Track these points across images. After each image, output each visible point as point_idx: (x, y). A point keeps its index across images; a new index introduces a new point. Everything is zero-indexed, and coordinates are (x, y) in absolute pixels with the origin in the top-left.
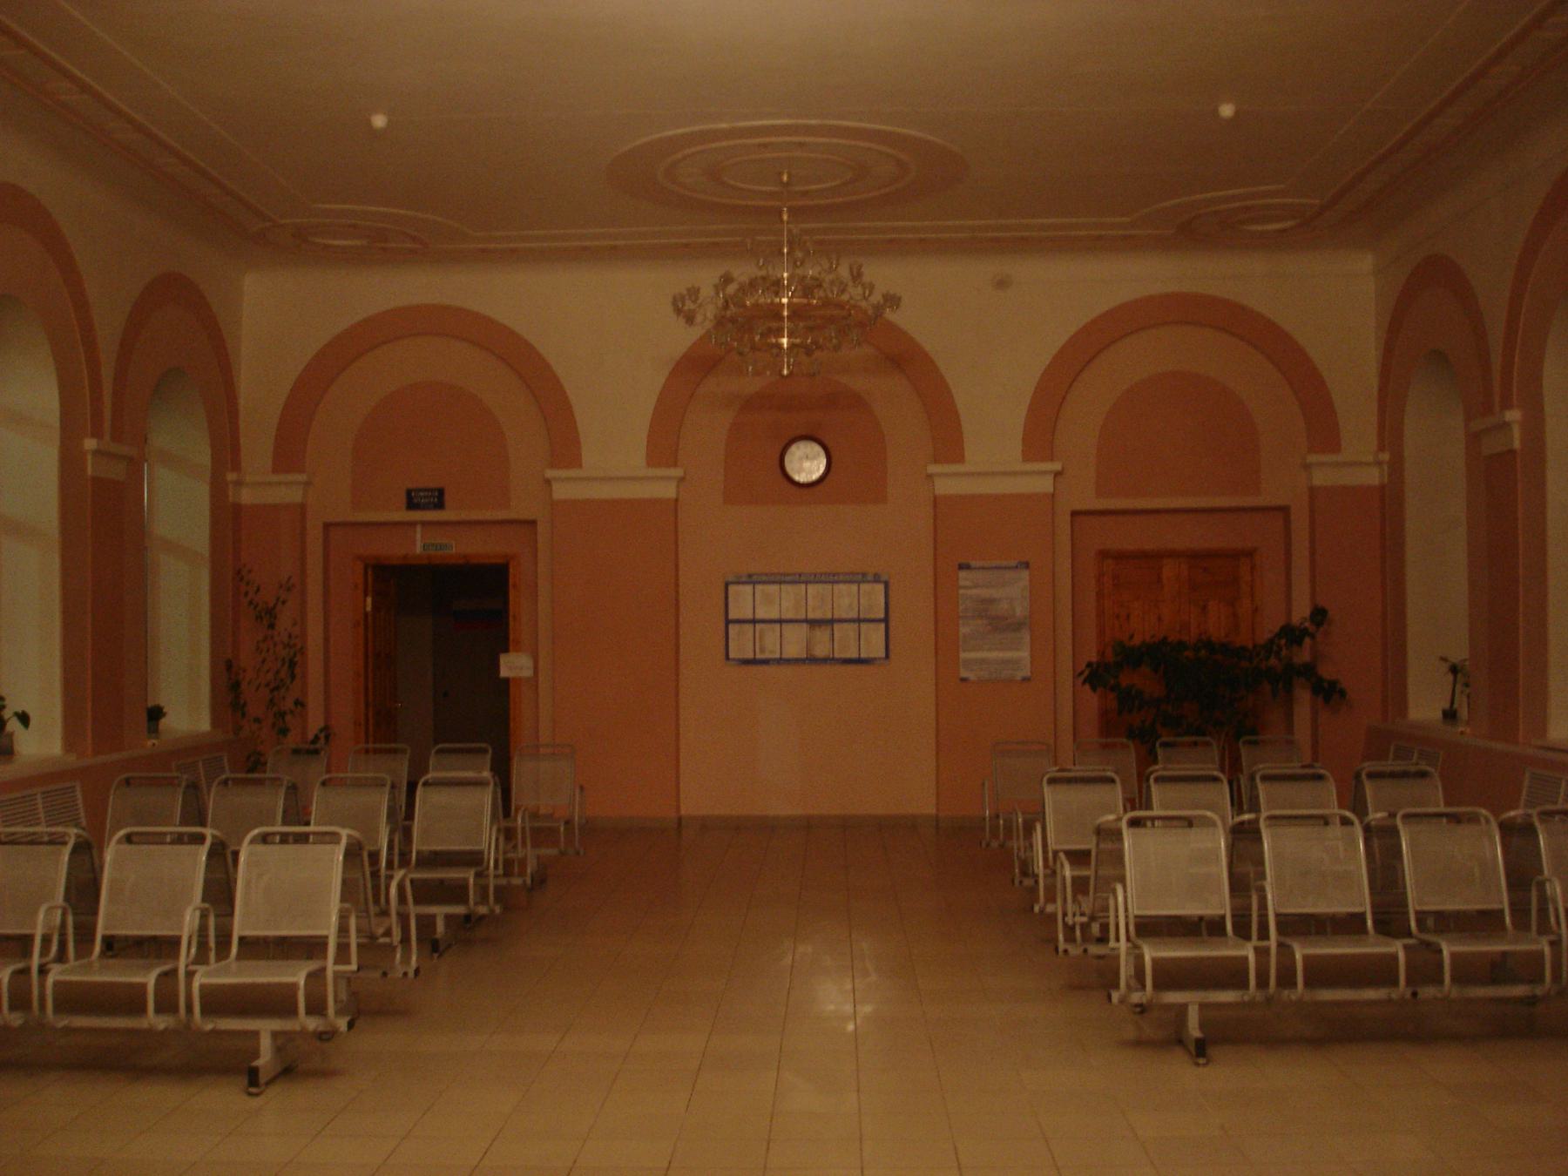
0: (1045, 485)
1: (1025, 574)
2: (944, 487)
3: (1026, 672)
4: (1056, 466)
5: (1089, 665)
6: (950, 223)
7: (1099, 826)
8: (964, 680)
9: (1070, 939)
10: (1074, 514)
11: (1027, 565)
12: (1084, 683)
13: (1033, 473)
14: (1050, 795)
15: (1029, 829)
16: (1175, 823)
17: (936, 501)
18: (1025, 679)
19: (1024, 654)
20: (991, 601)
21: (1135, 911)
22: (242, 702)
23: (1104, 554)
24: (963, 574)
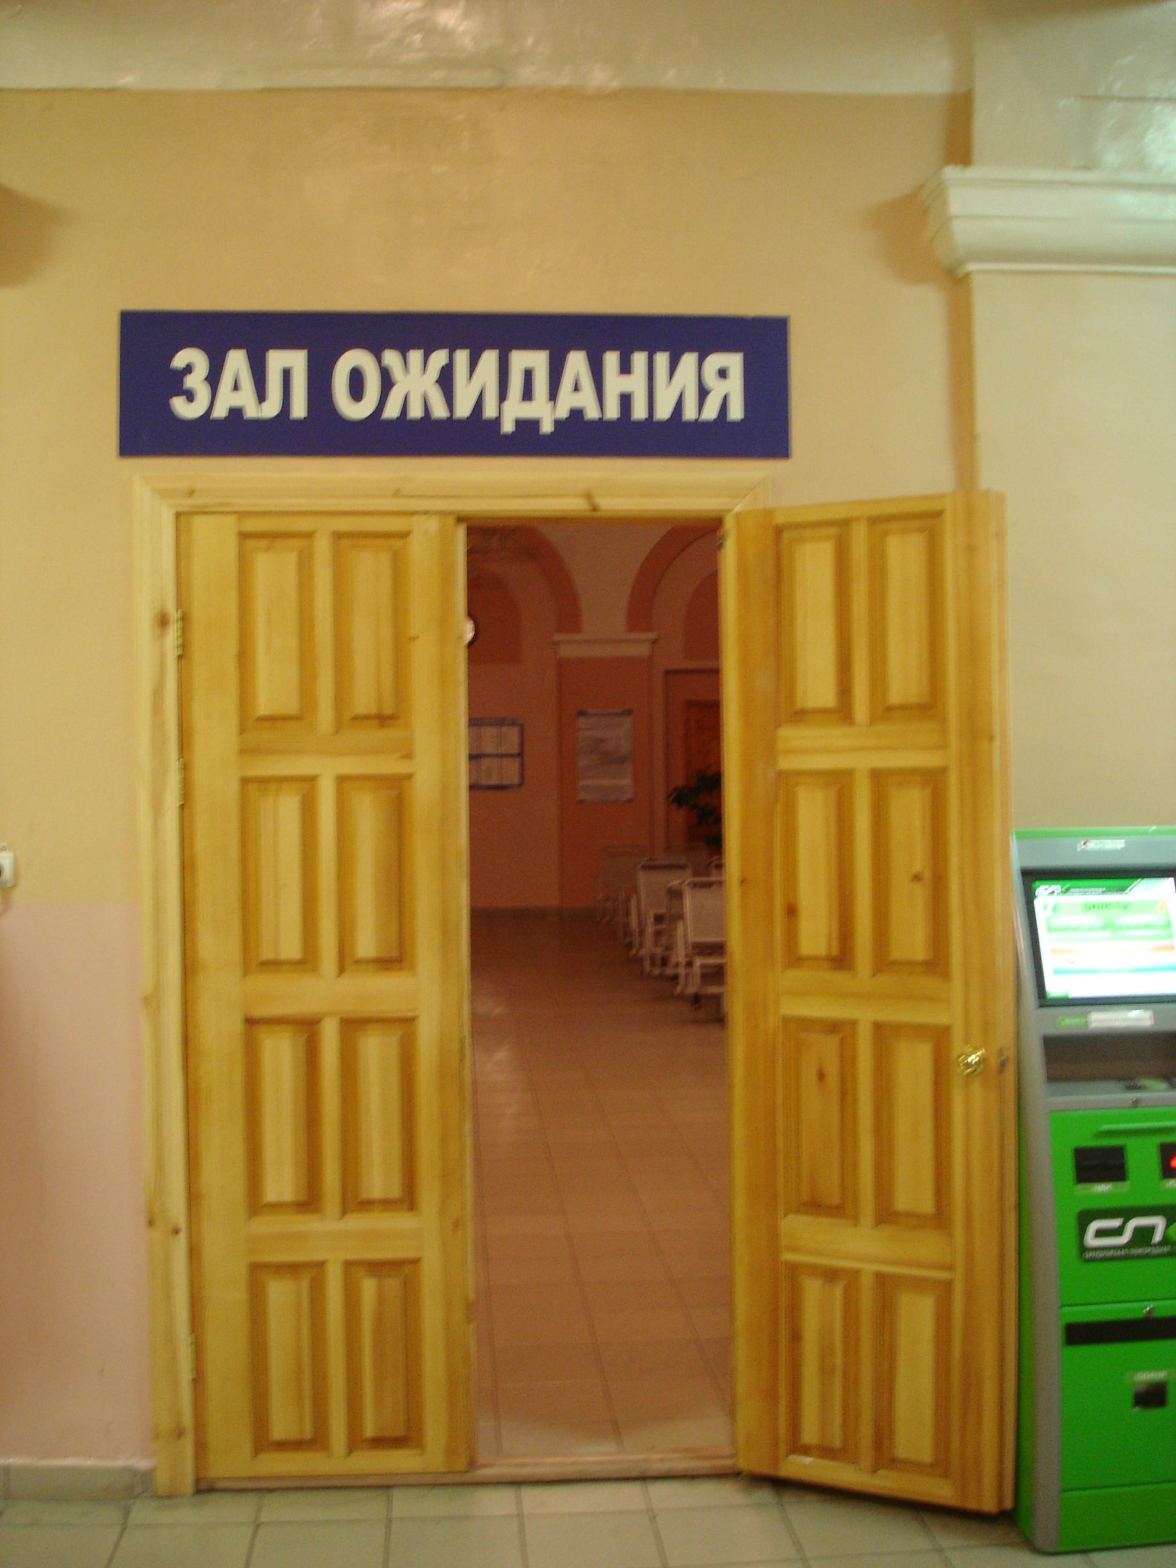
0: (643, 650)
1: (627, 722)
2: (568, 651)
3: (629, 795)
4: (652, 635)
5: (676, 789)
6: (1019, 920)
7: (671, 887)
8: (582, 802)
9: (653, 964)
10: (667, 672)
11: (629, 712)
12: (673, 802)
13: (1002, 1303)
14: (643, 878)
15: (628, 900)
16: (501, 408)
17: (561, 663)
18: (629, 801)
19: (627, 781)
20: (602, 740)
21: (692, 938)
22: (181, 760)
23: (689, 704)
24: (581, 719)
